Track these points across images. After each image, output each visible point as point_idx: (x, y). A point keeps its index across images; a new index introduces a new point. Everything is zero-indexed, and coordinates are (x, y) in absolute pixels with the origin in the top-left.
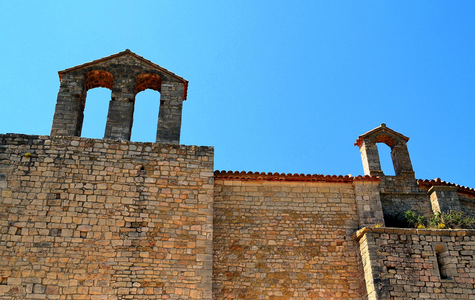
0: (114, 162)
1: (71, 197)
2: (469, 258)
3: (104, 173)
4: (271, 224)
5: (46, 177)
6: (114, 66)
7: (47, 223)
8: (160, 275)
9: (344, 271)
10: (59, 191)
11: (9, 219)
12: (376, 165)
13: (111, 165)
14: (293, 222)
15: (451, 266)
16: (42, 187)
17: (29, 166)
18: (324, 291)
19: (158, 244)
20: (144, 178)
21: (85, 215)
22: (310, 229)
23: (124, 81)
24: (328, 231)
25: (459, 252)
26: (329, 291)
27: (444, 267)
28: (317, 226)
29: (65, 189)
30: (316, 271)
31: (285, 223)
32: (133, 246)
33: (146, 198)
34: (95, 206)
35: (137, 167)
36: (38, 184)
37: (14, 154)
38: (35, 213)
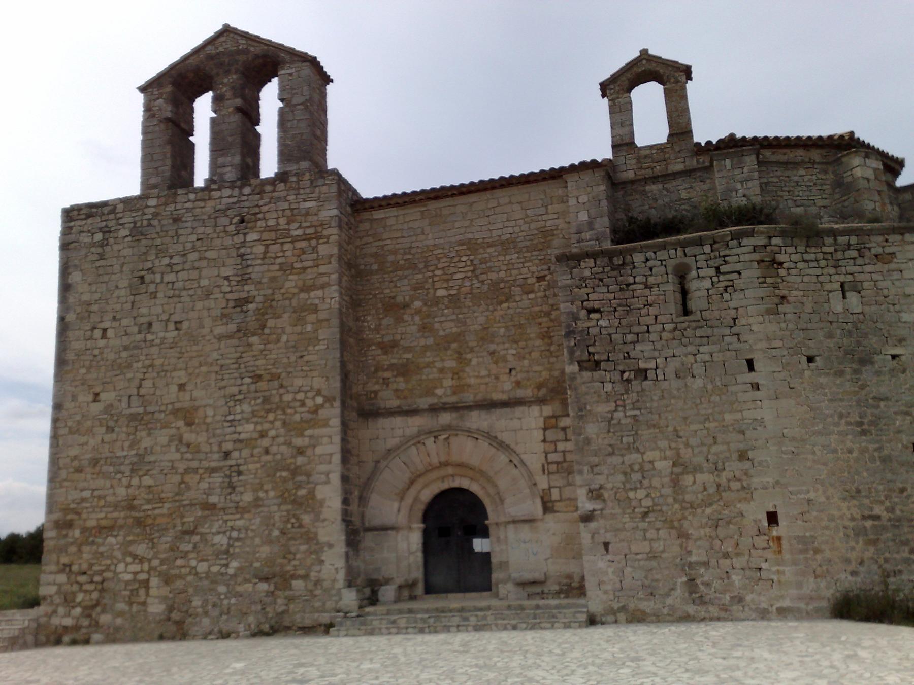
0: (204, 220)
1: (158, 278)
2: (735, 276)
3: (194, 238)
4: (440, 266)
5: (125, 257)
6: (210, 57)
7: (135, 318)
8: (274, 364)
9: (545, 319)
10: (143, 273)
11: (92, 320)
12: (623, 131)
13: (201, 224)
14: (472, 258)
15: (698, 294)
16: (121, 272)
17: (102, 246)
18: (514, 352)
19: (271, 323)
20: (245, 234)
21: (176, 300)
22: (496, 264)
23: (226, 80)
24: (523, 263)
25: (717, 269)
26: (521, 350)
27: (689, 296)
28: (508, 257)
29: (149, 269)
30: (503, 325)
31: (460, 261)
32: (239, 331)
33: (249, 262)
34: (188, 285)
35: (235, 221)
36: (117, 268)
37: (83, 232)
38: (118, 307)
